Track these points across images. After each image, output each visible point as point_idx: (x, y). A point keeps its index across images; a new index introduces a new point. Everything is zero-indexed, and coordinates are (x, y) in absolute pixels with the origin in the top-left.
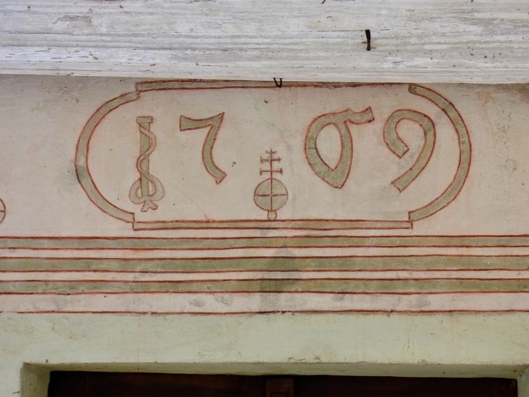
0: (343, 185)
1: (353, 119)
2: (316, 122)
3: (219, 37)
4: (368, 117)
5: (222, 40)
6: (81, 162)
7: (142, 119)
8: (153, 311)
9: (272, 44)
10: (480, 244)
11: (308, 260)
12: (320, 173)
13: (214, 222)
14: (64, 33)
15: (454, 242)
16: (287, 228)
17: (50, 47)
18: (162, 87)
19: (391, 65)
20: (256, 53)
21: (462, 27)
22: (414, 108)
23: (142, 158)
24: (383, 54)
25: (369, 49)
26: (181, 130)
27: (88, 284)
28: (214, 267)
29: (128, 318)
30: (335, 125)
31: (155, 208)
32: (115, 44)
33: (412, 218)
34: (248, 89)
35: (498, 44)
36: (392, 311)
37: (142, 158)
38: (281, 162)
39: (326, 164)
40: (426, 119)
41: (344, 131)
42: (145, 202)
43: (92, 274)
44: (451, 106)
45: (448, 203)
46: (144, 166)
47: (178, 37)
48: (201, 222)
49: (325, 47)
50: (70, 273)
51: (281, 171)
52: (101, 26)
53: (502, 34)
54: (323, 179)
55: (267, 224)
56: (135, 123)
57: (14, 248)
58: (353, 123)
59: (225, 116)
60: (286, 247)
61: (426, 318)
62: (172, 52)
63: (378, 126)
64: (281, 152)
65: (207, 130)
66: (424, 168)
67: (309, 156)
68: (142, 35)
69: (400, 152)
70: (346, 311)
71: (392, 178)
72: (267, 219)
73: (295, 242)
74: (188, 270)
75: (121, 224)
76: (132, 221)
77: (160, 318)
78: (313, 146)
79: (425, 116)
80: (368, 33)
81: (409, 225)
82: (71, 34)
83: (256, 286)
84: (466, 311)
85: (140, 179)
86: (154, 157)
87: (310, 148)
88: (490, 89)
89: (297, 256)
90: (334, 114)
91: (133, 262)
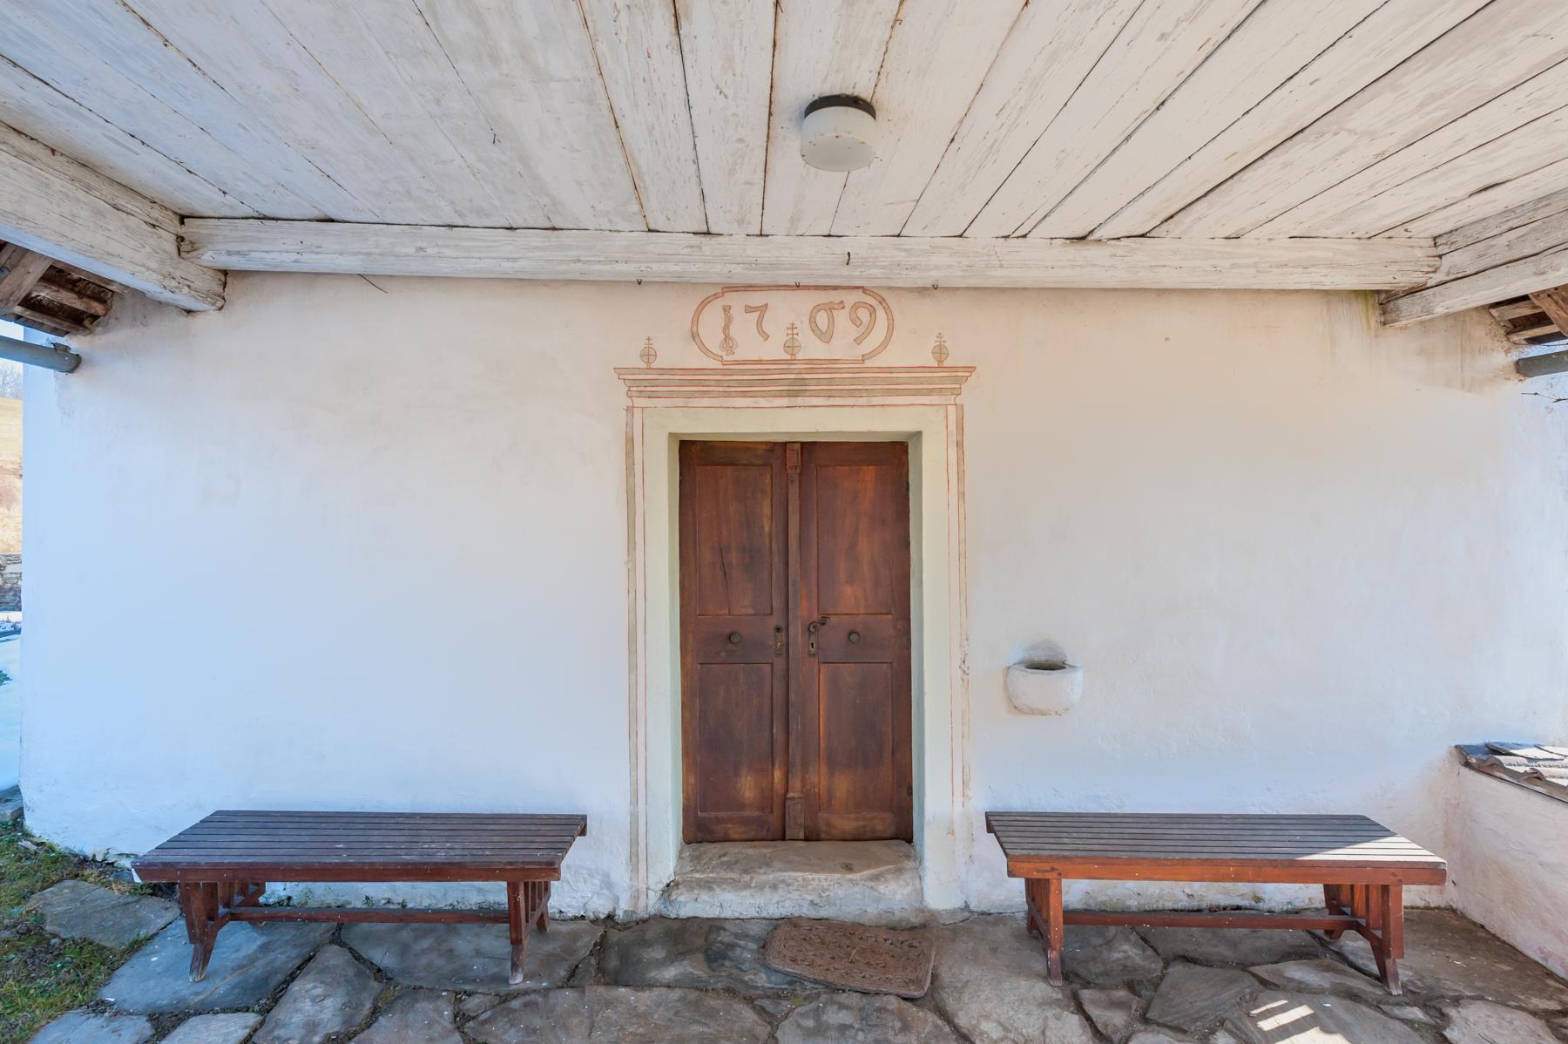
1: (834, 306)
4: (841, 306)
29: (720, 409)
30: (826, 310)
41: (829, 312)
46: (727, 331)
55: (790, 362)
63: (846, 311)
64: (797, 324)
65: (759, 312)
77: (737, 410)
80: (849, 254)
83: (785, 393)
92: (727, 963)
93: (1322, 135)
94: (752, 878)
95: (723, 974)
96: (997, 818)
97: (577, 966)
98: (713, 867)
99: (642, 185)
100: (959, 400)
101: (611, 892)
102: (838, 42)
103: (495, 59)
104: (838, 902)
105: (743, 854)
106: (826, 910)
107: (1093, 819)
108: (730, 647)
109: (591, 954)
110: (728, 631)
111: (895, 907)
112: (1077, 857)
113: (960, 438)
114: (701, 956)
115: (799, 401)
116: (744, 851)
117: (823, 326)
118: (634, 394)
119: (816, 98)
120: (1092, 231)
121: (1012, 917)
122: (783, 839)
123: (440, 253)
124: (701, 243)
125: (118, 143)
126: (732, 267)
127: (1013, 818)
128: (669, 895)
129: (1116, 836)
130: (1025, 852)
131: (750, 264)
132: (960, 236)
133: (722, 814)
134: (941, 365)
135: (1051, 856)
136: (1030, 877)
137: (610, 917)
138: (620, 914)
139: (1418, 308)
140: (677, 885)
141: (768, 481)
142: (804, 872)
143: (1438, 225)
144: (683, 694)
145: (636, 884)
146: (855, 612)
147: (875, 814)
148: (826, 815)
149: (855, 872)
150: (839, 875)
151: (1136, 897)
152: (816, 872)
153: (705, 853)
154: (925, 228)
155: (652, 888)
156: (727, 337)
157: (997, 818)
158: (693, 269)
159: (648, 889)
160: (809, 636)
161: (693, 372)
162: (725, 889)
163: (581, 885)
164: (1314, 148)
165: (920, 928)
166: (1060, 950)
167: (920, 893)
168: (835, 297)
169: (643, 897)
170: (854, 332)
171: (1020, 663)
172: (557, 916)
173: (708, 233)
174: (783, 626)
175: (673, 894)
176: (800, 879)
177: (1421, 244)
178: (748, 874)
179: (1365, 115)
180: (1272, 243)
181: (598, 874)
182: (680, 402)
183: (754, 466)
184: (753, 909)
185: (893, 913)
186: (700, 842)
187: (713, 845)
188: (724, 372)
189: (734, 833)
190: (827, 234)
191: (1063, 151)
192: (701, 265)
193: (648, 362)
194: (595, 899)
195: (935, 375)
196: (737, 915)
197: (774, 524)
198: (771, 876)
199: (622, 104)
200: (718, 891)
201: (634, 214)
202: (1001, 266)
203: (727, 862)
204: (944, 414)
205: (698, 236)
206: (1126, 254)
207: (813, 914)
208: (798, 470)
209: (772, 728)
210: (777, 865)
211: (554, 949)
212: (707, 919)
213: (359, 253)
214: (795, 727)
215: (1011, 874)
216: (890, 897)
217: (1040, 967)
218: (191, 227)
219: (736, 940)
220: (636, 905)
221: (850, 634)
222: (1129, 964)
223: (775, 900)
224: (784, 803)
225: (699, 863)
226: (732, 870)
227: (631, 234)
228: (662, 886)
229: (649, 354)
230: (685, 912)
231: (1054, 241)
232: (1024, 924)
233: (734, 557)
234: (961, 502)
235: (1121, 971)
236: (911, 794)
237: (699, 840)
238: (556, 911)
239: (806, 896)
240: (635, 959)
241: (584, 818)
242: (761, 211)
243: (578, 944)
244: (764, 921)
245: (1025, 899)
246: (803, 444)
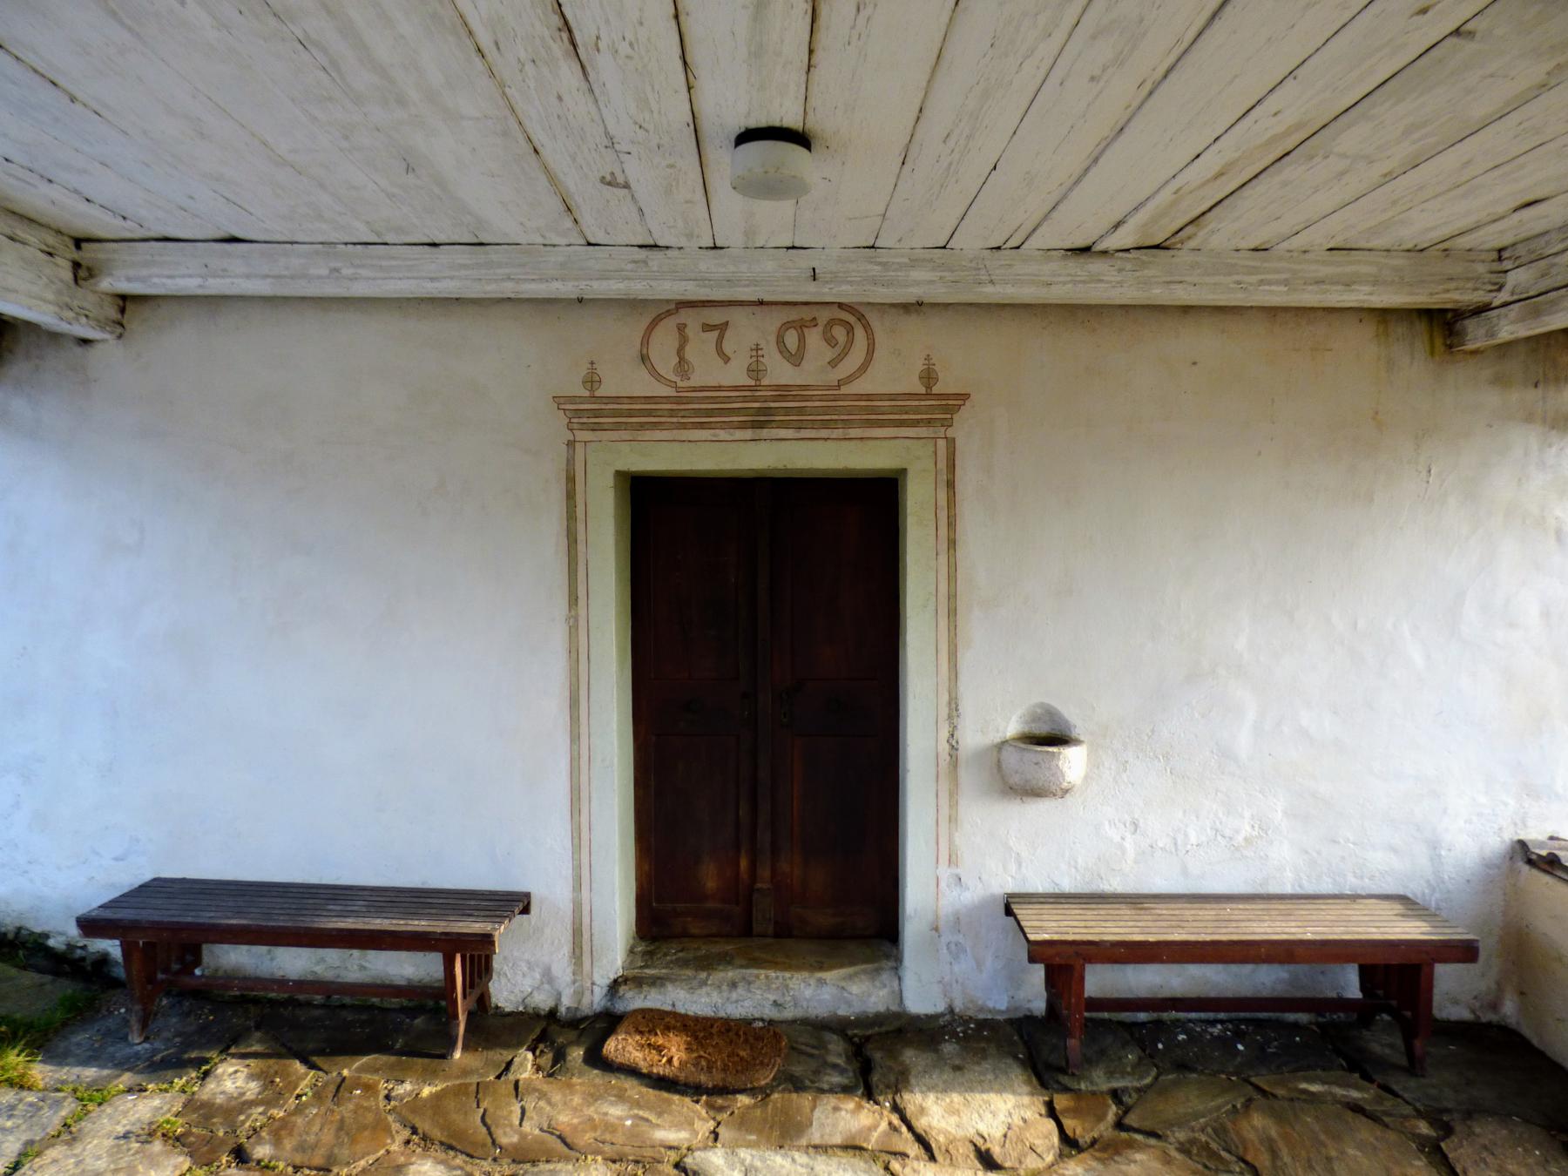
6: (645, 351)
15: (864, 398)
17: (624, 279)
19: (827, 290)
20: (747, 282)
21: (869, 267)
25: (814, 280)
31: (689, 379)
49: (789, 279)
51: (763, 356)
54: (788, 361)
55: (755, 388)
61: (847, 442)
63: (820, 328)
71: (828, 360)
77: (693, 444)
80: (814, 269)
83: (749, 424)
88: (886, 306)
93: (1311, 158)
100: (950, 433)
101: (552, 987)
102: (753, 86)
103: (402, 101)
106: (790, 1012)
115: (765, 433)
118: (575, 426)
119: (743, 130)
123: (356, 273)
124: (647, 257)
125: (18, 179)
128: (617, 991)
132: (944, 247)
134: (929, 391)
137: (553, 1013)
139: (1482, 331)
143: (1492, 237)
152: (781, 970)
155: (598, 983)
156: (682, 360)
159: (593, 984)
164: (1308, 170)
168: (806, 313)
169: (587, 993)
170: (830, 354)
177: (1483, 257)
179: (1351, 139)
180: (1307, 256)
181: (538, 966)
182: (625, 435)
184: (709, 1008)
188: (678, 400)
190: (791, 245)
193: (592, 390)
199: (540, 137)
202: (992, 282)
205: (644, 249)
210: (738, 961)
213: (267, 276)
218: (89, 253)
220: (579, 1002)
227: (569, 248)
229: (592, 381)
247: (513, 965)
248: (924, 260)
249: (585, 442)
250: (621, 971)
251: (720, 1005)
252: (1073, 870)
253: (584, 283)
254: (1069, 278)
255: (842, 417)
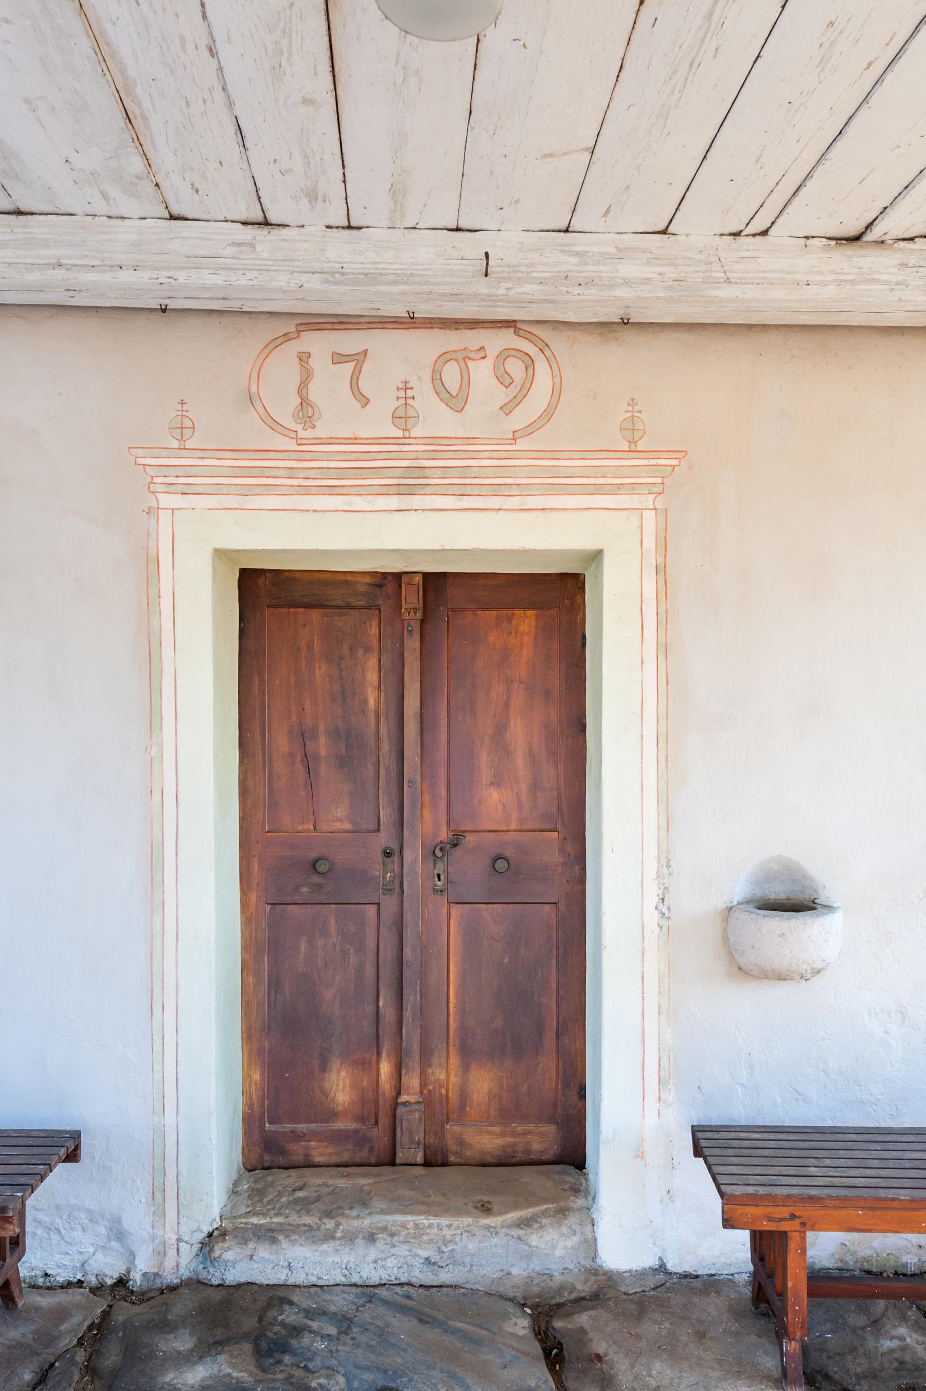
0: (462, 410)
2: (441, 358)
3: (363, 263)
4: (482, 354)
5: (365, 266)
6: (254, 389)
7: (302, 354)
8: (314, 509)
9: (407, 270)
10: (567, 457)
11: (435, 469)
12: (445, 399)
13: (360, 438)
14: (233, 258)
16: (418, 444)
18: (317, 328)
19: (504, 292)
21: (562, 258)
22: (517, 348)
23: (302, 386)
24: (498, 280)
25: (486, 275)
26: (333, 364)
27: (262, 487)
28: (361, 475)
30: (456, 360)
31: (314, 427)
32: (275, 268)
33: (515, 436)
34: (387, 330)
35: (591, 273)
36: (499, 509)
37: (302, 386)
38: (414, 390)
39: (449, 393)
40: (527, 357)
41: (463, 365)
42: (305, 422)
43: (265, 479)
44: (547, 347)
45: (543, 425)
47: (328, 262)
48: (350, 439)
50: (247, 478)
52: (263, 251)
53: (594, 265)
54: (447, 405)
55: (403, 441)
56: (296, 357)
57: (202, 458)
58: (470, 359)
59: (368, 351)
60: (417, 459)
61: (525, 514)
62: (324, 276)
63: (489, 362)
65: (354, 363)
66: (525, 396)
67: (435, 386)
68: (299, 261)
69: (507, 383)
70: (464, 509)
72: (402, 436)
73: (425, 455)
74: (341, 477)
75: (288, 439)
76: (295, 437)
77: (321, 514)
78: (439, 377)
79: (526, 354)
80: (487, 254)
81: (513, 442)
82: (237, 258)
83: (394, 490)
84: (556, 509)
85: (301, 403)
86: (311, 386)
87: (436, 380)
89: (426, 466)
90: (455, 351)
91: (297, 470)
92: (287, 1359)
94: (338, 1225)
95: (280, 1376)
96: (709, 1135)
97: (52, 1365)
98: (280, 1209)
99: (138, 112)
101: (123, 1245)
104: (467, 1260)
105: (328, 1186)
107: (853, 1137)
108: (316, 879)
109: (80, 1342)
110: (314, 855)
111: (553, 1267)
112: (830, 1197)
113: (661, 560)
114: (247, 1347)
115: (416, 501)
116: (331, 1182)
117: (454, 388)
118: (160, 488)
120: (872, 223)
121: (730, 1282)
122: (392, 1163)
126: (304, 278)
127: (733, 1135)
128: (211, 1250)
129: (891, 1164)
130: (750, 1190)
131: (333, 274)
132: (664, 232)
133: (302, 1127)
134: (633, 448)
135: (789, 1196)
136: (758, 1227)
137: (122, 1282)
138: (136, 1278)
140: (223, 1234)
141: (374, 630)
142: (418, 1214)
144: (245, 948)
145: (162, 1233)
146: (504, 828)
147: (531, 1127)
148: (457, 1129)
149: (496, 1215)
150: (470, 1220)
151: (917, 1251)
153: (272, 1184)
154: (607, 212)
155: (186, 1239)
156: (305, 402)
157: (709, 1135)
158: (243, 281)
160: (435, 864)
161: (252, 455)
162: (296, 1240)
163: (77, 1234)
165: (591, 1300)
166: (802, 1340)
167: (591, 1245)
169: (172, 1253)
170: (502, 395)
171: (748, 902)
172: (40, 1281)
173: (266, 223)
174: (395, 847)
175: (216, 1248)
176: (412, 1224)
178: (332, 1218)
181: (103, 1218)
183: (353, 608)
184: (339, 1270)
185: (551, 1276)
186: (268, 1168)
187: (284, 1174)
189: (322, 1155)
191: (831, 24)
192: (256, 273)
193: (181, 439)
194: (100, 1255)
195: (625, 463)
196: (313, 1280)
197: (382, 694)
198: (366, 1222)
200: (284, 1243)
201: (137, 177)
202: (728, 281)
203: (304, 1199)
204: (638, 524)
206: (922, 264)
207: (428, 1278)
208: (419, 615)
209: (378, 1001)
210: (378, 1203)
211: (24, 1335)
212: (268, 1285)
214: (412, 998)
215: (728, 1223)
216: (545, 1252)
217: (770, 1363)
219: (305, 1320)
220: (161, 1264)
221: (495, 860)
222: (907, 1358)
223: (371, 1258)
224: (394, 1111)
225: (261, 1201)
226: (308, 1212)
228: (200, 1236)
230: (234, 1276)
231: (811, 241)
232: (747, 1292)
233: (322, 746)
234: (662, 658)
235: (896, 1369)
236: (582, 1097)
237: (266, 1165)
238: (38, 1273)
239: (419, 1251)
240: (144, 1351)
241: (76, 1136)
242: (341, 171)
243: (62, 1328)
244: (354, 1290)
245: (749, 1255)
246: (426, 576)
247: (69, 1216)
248: (637, 249)
249: (173, 509)
250: (218, 1219)
251: (353, 1266)
252: (822, 1074)
253: (166, 274)
254: (833, 277)
255: (518, 481)
